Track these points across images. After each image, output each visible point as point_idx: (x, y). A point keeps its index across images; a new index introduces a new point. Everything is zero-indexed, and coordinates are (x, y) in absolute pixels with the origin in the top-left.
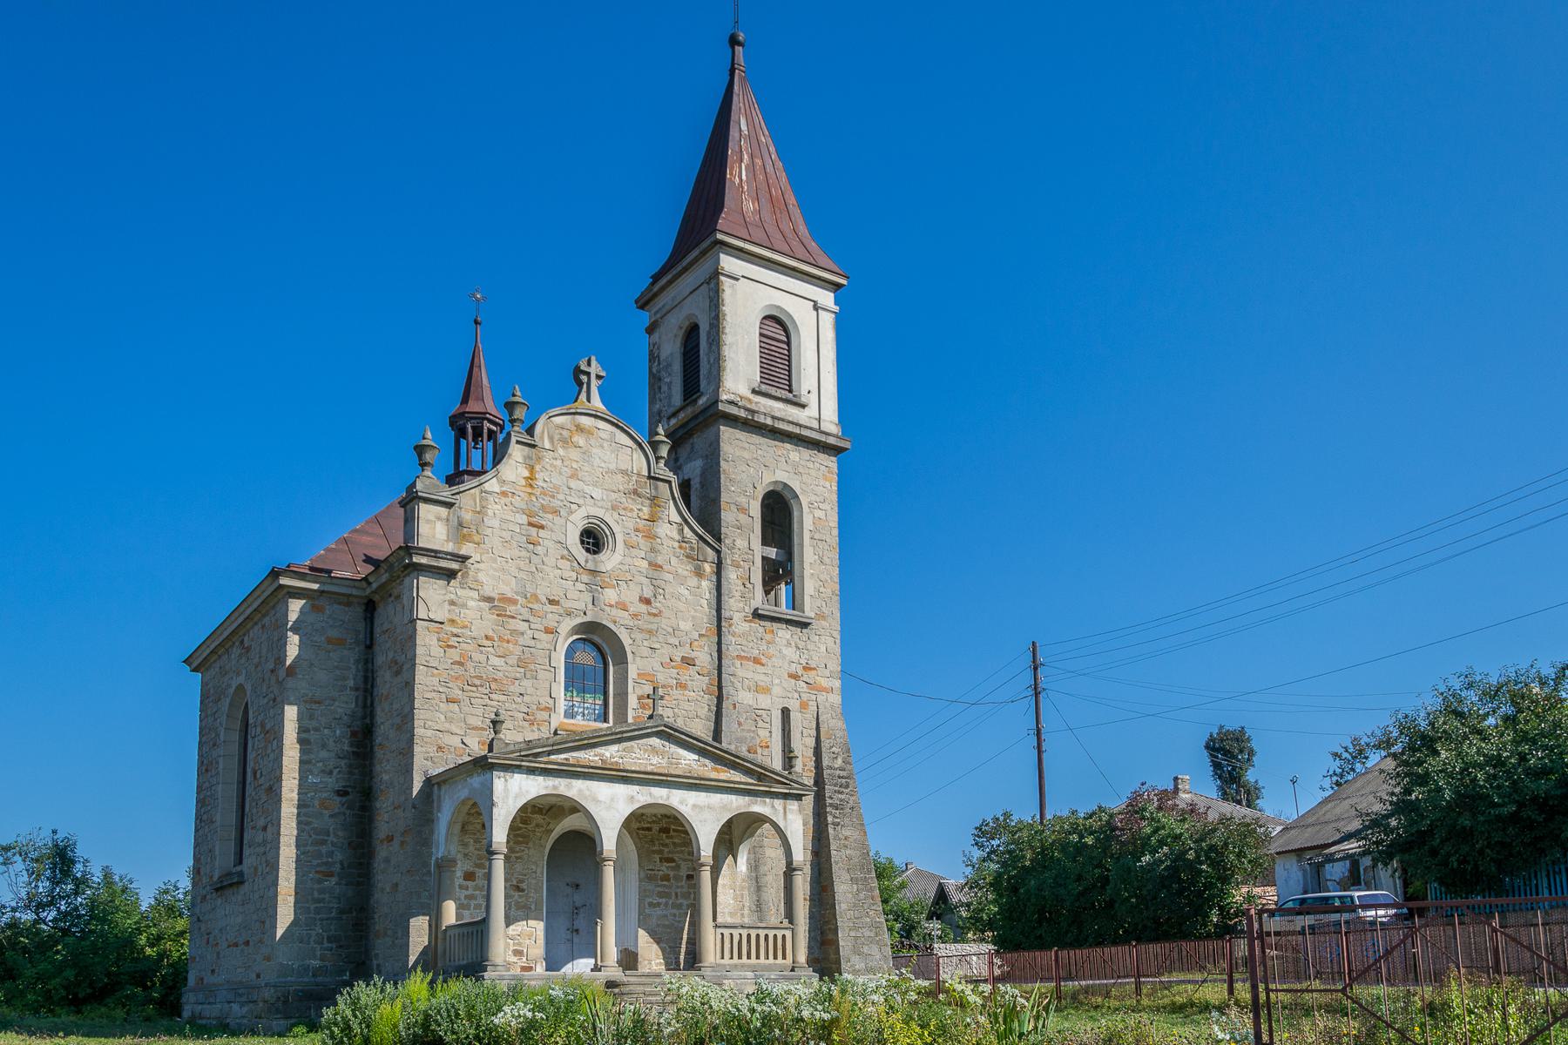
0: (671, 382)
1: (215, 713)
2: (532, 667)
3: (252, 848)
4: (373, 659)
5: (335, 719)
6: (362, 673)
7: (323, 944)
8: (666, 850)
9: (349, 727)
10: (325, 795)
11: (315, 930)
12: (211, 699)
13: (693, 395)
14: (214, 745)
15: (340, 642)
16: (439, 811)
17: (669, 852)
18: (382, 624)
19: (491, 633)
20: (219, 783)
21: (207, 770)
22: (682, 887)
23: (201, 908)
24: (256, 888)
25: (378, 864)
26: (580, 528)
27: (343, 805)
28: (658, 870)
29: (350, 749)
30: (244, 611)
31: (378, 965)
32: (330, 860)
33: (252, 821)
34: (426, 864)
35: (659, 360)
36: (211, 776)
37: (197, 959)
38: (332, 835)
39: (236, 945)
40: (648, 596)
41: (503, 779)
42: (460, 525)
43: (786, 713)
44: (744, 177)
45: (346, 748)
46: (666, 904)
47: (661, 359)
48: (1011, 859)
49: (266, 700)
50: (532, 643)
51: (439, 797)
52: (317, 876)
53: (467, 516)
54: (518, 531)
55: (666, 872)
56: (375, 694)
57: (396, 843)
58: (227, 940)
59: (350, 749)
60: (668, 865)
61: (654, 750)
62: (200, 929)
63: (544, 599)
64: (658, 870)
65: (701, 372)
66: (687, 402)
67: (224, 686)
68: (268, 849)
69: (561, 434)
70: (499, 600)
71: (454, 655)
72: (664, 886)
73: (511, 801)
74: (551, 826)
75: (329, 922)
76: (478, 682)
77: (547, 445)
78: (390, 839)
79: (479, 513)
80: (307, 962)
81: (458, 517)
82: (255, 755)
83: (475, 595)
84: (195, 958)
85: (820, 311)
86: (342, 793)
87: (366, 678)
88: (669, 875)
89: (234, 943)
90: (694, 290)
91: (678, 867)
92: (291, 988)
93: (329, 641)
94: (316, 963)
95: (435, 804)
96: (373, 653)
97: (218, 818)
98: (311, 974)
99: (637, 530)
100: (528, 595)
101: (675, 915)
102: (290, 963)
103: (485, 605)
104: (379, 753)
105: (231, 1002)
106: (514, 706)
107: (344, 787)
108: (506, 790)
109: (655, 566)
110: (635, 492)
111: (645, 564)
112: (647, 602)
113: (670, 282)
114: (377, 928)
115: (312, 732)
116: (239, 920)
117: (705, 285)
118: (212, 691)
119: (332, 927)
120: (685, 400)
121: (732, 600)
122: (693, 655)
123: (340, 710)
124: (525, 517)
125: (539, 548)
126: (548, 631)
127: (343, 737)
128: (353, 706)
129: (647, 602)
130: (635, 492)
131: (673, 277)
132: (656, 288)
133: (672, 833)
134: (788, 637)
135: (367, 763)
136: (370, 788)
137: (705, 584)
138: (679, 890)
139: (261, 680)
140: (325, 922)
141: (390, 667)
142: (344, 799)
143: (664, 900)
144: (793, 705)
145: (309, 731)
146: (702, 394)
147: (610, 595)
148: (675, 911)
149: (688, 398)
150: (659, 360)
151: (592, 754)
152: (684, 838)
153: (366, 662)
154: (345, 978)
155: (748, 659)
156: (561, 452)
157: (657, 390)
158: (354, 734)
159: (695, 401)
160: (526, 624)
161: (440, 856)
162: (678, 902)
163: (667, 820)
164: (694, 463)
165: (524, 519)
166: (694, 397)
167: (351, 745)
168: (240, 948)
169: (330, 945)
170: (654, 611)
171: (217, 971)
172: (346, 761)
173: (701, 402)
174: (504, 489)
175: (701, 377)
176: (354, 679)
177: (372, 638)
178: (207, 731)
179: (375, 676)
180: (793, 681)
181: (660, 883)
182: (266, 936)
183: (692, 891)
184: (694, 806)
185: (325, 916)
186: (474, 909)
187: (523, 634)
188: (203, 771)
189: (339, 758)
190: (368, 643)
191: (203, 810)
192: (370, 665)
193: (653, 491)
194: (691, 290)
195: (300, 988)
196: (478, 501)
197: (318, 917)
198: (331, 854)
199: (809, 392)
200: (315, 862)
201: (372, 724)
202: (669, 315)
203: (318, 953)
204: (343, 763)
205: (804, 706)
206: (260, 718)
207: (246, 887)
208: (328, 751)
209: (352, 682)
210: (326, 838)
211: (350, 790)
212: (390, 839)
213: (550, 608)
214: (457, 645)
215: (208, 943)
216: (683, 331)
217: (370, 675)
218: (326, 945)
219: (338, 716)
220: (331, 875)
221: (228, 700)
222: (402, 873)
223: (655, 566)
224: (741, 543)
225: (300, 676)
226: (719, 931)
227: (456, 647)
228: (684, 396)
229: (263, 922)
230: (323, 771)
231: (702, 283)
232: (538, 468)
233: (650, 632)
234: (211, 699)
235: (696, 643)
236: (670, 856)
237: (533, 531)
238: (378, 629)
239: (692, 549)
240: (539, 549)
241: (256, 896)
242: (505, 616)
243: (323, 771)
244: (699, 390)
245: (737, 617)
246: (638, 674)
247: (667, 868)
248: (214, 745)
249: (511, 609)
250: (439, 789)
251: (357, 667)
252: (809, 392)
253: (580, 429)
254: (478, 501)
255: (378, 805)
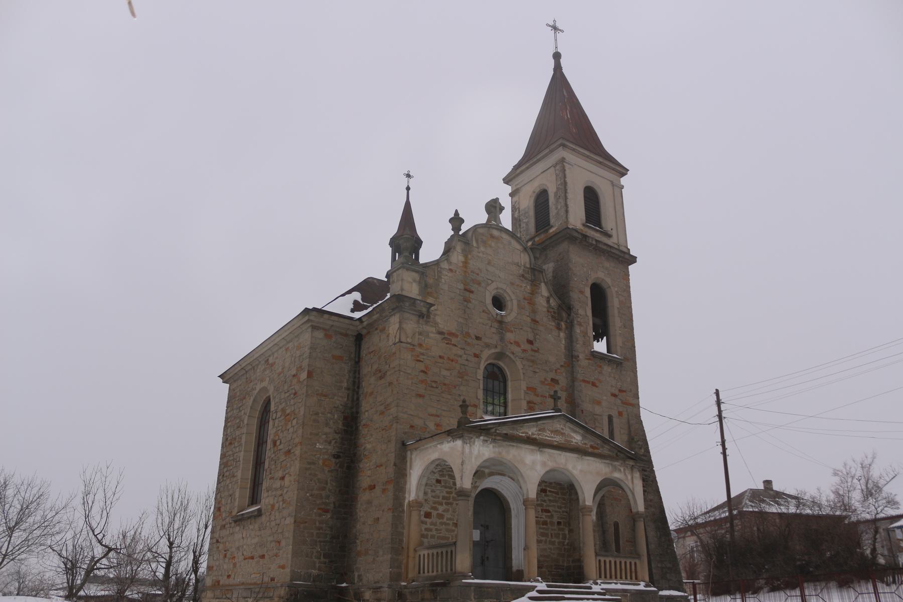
0: (528, 222)
1: (240, 407)
2: (466, 377)
3: (270, 492)
4: (359, 371)
5: (335, 407)
6: (352, 379)
7: (320, 559)
8: (545, 504)
9: (343, 413)
10: (326, 457)
11: (315, 548)
12: (237, 399)
13: (545, 227)
14: (238, 427)
15: (340, 358)
16: (411, 468)
17: (547, 506)
18: (368, 348)
19: (442, 354)
20: (241, 451)
21: (231, 444)
22: (555, 530)
23: (220, 534)
24: (272, 518)
25: (361, 506)
26: (492, 295)
27: (337, 464)
28: (541, 518)
29: (343, 428)
30: (267, 345)
31: (359, 576)
32: (327, 501)
33: (271, 474)
34: (402, 505)
35: (519, 210)
36: (234, 448)
37: (215, 568)
38: (329, 484)
39: (252, 558)
40: (531, 339)
41: (468, 445)
42: (426, 286)
43: (610, 418)
44: (569, 116)
45: (340, 427)
46: (546, 542)
47: (520, 209)
48: (841, 518)
49: (287, 394)
50: (466, 363)
51: (411, 459)
52: (320, 511)
53: (431, 281)
54: (458, 293)
55: (546, 519)
56: (360, 392)
57: (378, 490)
58: (243, 555)
59: (343, 428)
60: (546, 514)
61: (556, 432)
62: (218, 547)
63: (474, 337)
64: (541, 518)
65: (551, 215)
66: (538, 233)
67: (249, 389)
68: (285, 491)
69: (482, 239)
70: (448, 334)
71: (421, 366)
72: (543, 528)
73: (473, 460)
74: (477, 484)
75: (324, 544)
76: (434, 385)
77: (475, 244)
78: (372, 487)
79: (436, 280)
80: (310, 571)
81: (425, 281)
82: (275, 431)
83: (434, 330)
84: (213, 567)
85: (615, 187)
86: (336, 456)
87: (354, 382)
88: (547, 521)
89: (252, 557)
90: (544, 171)
91: (552, 516)
92: (299, 589)
93: (334, 357)
94: (315, 572)
95: (408, 464)
96: (359, 366)
97: (239, 474)
98: (312, 580)
99: (525, 299)
100: (464, 332)
101: (551, 549)
102: (299, 571)
103: (438, 336)
104: (364, 431)
105: (246, 598)
106: (456, 402)
107: (338, 452)
108: (471, 452)
109: (535, 321)
110: (523, 276)
111: (529, 319)
112: (530, 342)
113: (528, 168)
114: (359, 549)
115: (320, 415)
116: (256, 540)
117: (552, 169)
118: (238, 394)
119: (327, 548)
120: (537, 232)
121: (578, 345)
122: (557, 378)
123: (337, 402)
124: (462, 285)
125: (470, 304)
126: (476, 356)
127: (339, 419)
128: (346, 399)
129: (530, 342)
130: (523, 276)
131: (530, 165)
132: (518, 171)
133: (548, 493)
134: (610, 370)
135: (353, 437)
136: (355, 455)
137: (562, 335)
138: (553, 532)
139: (284, 382)
140: (322, 543)
141: (374, 374)
142: (337, 461)
143: (543, 538)
144: (614, 413)
145: (319, 414)
146: (552, 227)
147: (509, 336)
148: (551, 546)
149: (538, 231)
150: (519, 210)
151: (521, 431)
152: (555, 497)
153: (355, 372)
154: (333, 584)
155: (588, 382)
156: (482, 249)
157: (518, 226)
158: (345, 418)
159: (547, 230)
160: (463, 351)
161: (411, 499)
162: (553, 540)
163: (545, 484)
164: (547, 265)
165: (461, 286)
166: (547, 228)
167: (344, 425)
168: (255, 560)
169: (325, 560)
170: (536, 349)
171: (233, 576)
172: (340, 435)
173: (551, 231)
174: (450, 267)
175: (551, 217)
176: (347, 383)
177: (359, 357)
178: (233, 418)
179: (361, 381)
180: (614, 398)
181: (542, 526)
182: (281, 551)
183: (561, 532)
184: (581, 471)
185: (322, 539)
186: (431, 538)
187: (461, 356)
188: (227, 444)
189: (336, 433)
190: (357, 360)
191: (225, 470)
192: (357, 374)
193: (533, 277)
194: (542, 171)
195: (306, 589)
196: (436, 273)
197: (318, 540)
198: (328, 497)
199: (612, 229)
200: (318, 502)
201: (357, 413)
202: (525, 186)
203: (317, 565)
204: (337, 436)
205: (620, 414)
206: (280, 407)
207: (264, 518)
208: (329, 428)
209: (346, 384)
210: (325, 486)
211: (341, 455)
212: (372, 487)
213: (475, 342)
214: (422, 360)
215: (225, 556)
216: (535, 194)
217: (357, 381)
218: (322, 559)
219: (336, 406)
220: (327, 511)
221: (252, 399)
222: (383, 511)
223: (535, 321)
224: (581, 312)
225: (316, 379)
226: (598, 558)
227: (422, 362)
228: (536, 229)
229: (279, 542)
230: (326, 441)
231: (551, 167)
232: (469, 256)
233: (533, 361)
234: (237, 399)
235: (559, 371)
236: (547, 508)
237: (467, 293)
238: (364, 352)
239: (555, 313)
240: (470, 305)
241: (273, 524)
242: (451, 344)
243: (326, 441)
244: (549, 224)
245: (581, 356)
246: (527, 388)
247: (546, 516)
248: (238, 427)
249: (454, 340)
250: (411, 454)
251: (349, 375)
252: (612, 229)
253: (492, 236)
254: (436, 273)
255: (361, 466)
